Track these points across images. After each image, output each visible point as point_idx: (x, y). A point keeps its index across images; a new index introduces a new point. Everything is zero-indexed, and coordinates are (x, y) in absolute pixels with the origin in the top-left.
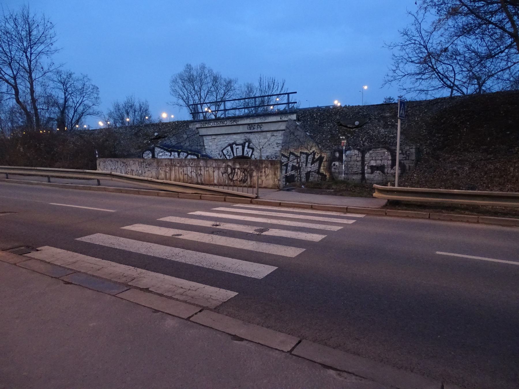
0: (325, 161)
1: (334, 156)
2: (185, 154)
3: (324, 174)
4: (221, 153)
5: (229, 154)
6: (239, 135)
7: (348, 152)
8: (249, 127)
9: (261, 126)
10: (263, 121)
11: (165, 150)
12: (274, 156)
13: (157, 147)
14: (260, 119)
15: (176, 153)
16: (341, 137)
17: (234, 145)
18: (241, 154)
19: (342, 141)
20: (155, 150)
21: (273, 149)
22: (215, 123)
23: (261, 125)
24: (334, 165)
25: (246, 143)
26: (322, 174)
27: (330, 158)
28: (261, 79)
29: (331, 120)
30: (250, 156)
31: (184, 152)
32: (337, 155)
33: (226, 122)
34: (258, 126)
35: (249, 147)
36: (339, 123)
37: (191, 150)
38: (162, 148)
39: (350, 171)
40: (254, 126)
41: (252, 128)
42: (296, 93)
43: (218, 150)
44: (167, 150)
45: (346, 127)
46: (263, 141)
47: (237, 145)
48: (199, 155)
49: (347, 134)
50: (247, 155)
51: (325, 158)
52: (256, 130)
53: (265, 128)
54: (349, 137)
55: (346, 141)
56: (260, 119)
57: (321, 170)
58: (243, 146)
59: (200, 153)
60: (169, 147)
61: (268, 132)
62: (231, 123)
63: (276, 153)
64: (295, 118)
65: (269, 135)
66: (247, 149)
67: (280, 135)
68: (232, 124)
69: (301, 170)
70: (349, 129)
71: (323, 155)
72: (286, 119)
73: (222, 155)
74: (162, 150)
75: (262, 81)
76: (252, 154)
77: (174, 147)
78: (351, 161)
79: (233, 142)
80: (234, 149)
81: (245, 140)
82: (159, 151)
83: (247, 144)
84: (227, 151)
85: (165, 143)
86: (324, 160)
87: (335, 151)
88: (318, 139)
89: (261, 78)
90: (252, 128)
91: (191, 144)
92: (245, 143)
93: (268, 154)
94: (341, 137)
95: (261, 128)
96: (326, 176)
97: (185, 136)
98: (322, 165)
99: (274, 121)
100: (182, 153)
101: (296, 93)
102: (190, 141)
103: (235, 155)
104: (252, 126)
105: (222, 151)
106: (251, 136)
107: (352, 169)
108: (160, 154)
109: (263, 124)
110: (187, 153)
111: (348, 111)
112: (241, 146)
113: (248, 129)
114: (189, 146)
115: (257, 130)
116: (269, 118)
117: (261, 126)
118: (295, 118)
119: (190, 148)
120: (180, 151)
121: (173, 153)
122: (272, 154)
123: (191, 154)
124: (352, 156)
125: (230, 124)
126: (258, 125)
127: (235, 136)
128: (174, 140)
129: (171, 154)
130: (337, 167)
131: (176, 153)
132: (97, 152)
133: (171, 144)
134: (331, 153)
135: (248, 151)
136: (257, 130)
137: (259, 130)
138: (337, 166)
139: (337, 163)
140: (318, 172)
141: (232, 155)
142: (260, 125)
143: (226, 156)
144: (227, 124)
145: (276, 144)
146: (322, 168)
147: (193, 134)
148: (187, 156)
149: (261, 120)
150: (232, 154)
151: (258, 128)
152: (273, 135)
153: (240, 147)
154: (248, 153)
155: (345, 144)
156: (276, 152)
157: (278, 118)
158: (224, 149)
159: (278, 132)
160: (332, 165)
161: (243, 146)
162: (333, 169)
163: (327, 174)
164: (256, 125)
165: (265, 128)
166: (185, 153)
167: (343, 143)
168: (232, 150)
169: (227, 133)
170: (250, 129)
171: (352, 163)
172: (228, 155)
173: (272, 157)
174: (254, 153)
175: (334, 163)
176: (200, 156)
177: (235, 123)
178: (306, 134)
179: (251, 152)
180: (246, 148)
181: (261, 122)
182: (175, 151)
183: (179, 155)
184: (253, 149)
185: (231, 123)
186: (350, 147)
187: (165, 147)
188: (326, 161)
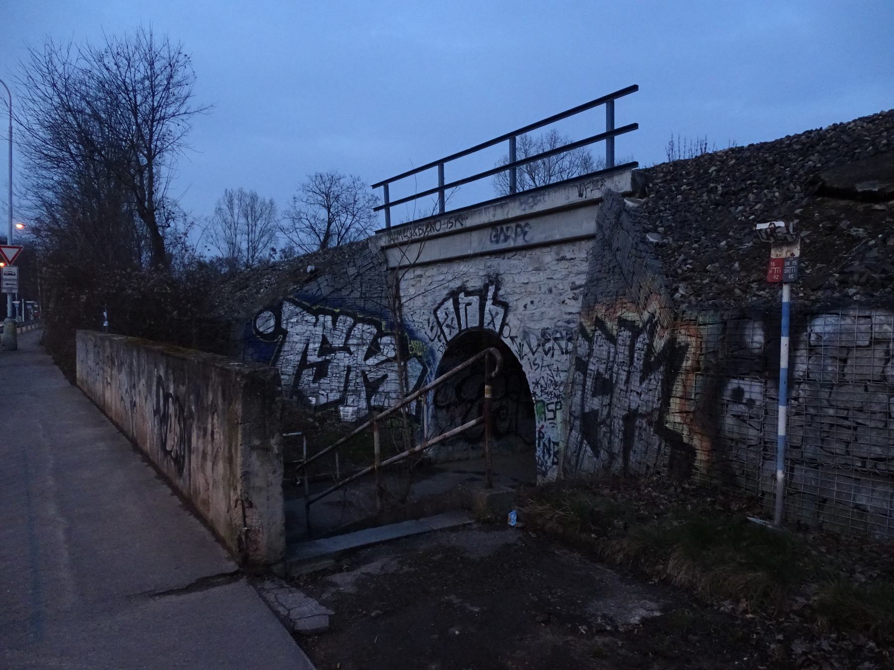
0: (687, 372)
1: (742, 345)
2: (350, 320)
3: (685, 440)
4: (432, 318)
5: (449, 322)
6: (471, 263)
7: (822, 326)
8: (494, 233)
9: (527, 229)
10: (528, 211)
11: (305, 308)
12: (564, 333)
13: (290, 300)
14: (521, 204)
15: (329, 318)
16: (760, 226)
17: (462, 295)
18: (477, 324)
19: (774, 254)
20: (284, 308)
21: (563, 307)
22: (417, 231)
23: (527, 225)
24: (738, 394)
25: (490, 287)
26: (672, 438)
27: (715, 353)
28: (673, 145)
29: (778, 178)
30: (497, 330)
31: (347, 314)
32: (757, 338)
33: (438, 227)
34: (519, 230)
35: (496, 302)
36: (813, 183)
37: (363, 310)
38: (297, 304)
39: (839, 448)
40: (508, 229)
41: (502, 237)
42: (634, 88)
43: (426, 311)
44: (310, 308)
45: (848, 194)
46: (533, 279)
47: (468, 294)
48: (384, 323)
49: (849, 227)
50: (491, 327)
51: (692, 350)
52: (511, 244)
53: (537, 233)
54: (858, 239)
55: (797, 252)
56: (521, 204)
57: (670, 418)
58: (482, 294)
59: (386, 319)
60: (314, 300)
61: (548, 249)
62: (450, 225)
63: (568, 322)
64: (628, 188)
65: (548, 257)
66: (492, 307)
67: (583, 255)
68: (452, 229)
69: (615, 400)
70: (860, 207)
71: (682, 339)
72: (597, 194)
73: (435, 323)
74: (298, 310)
75: (676, 149)
76: (504, 324)
77: (325, 300)
78: (843, 383)
79: (457, 284)
80: (460, 306)
81: (488, 276)
82: (292, 311)
83: (492, 289)
84: (446, 314)
85: (306, 291)
86: (687, 364)
87: (744, 316)
88: (688, 256)
89: (672, 143)
90: (502, 237)
91: (365, 294)
92: (486, 287)
93: (545, 324)
94: (760, 226)
95: (525, 233)
96: (692, 451)
97: (352, 271)
98: (678, 389)
99: (409, 170)
100: (341, 317)
101: (634, 88)
102: (364, 285)
103: (463, 327)
104: (502, 229)
105: (435, 311)
106: (501, 265)
107: (846, 435)
108: (292, 321)
109: (532, 222)
110: (353, 316)
111: (868, 130)
112: (478, 297)
113: (491, 241)
114: (361, 298)
115: (515, 240)
116: (546, 197)
117: (527, 229)
118: (628, 188)
119: (361, 303)
120: (338, 311)
121: (321, 318)
122: (560, 324)
123: (363, 321)
124: (849, 349)
125: (447, 230)
126: (517, 226)
127: (462, 268)
128: (326, 283)
129: (317, 320)
130: (755, 411)
131: (329, 318)
132: (105, 314)
133: (319, 293)
134: (724, 329)
135: (494, 313)
136: (515, 240)
137: (520, 242)
138: (751, 403)
139: (753, 389)
140: (660, 427)
141: (457, 326)
142: (523, 223)
143: (444, 328)
144: (441, 231)
145: (572, 289)
146: (675, 404)
147: (371, 265)
148: (354, 325)
149: (523, 207)
150: (455, 322)
151: (516, 233)
152: (563, 258)
153: (475, 299)
154: (492, 321)
155: (790, 271)
156: (569, 317)
157: (571, 196)
158: (438, 308)
159: (578, 244)
160: (727, 396)
161: (482, 294)
162: (729, 421)
163: (696, 442)
164: (513, 225)
165: (537, 233)
166: (348, 319)
167: (781, 262)
168: (457, 310)
169: (442, 257)
170: (497, 242)
171: (852, 396)
172: (448, 326)
173: (558, 335)
174: (511, 318)
175: (734, 384)
176: (386, 327)
177: (458, 226)
178: (645, 238)
179: (500, 317)
180: (489, 303)
181: (523, 213)
182: (325, 313)
183: (334, 322)
184: (506, 306)
185: (450, 225)
186: (852, 291)
187: (305, 301)
188: (695, 369)
